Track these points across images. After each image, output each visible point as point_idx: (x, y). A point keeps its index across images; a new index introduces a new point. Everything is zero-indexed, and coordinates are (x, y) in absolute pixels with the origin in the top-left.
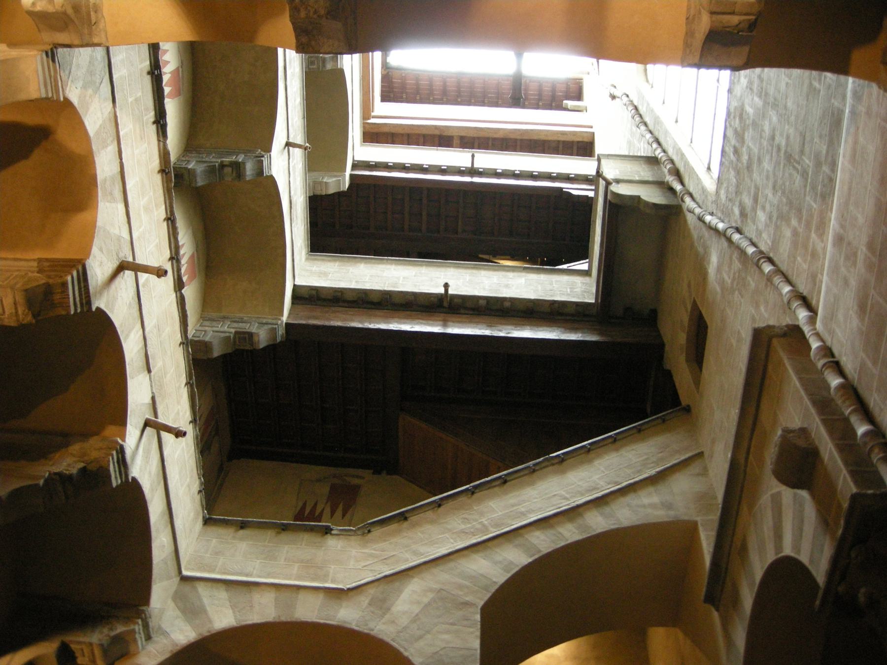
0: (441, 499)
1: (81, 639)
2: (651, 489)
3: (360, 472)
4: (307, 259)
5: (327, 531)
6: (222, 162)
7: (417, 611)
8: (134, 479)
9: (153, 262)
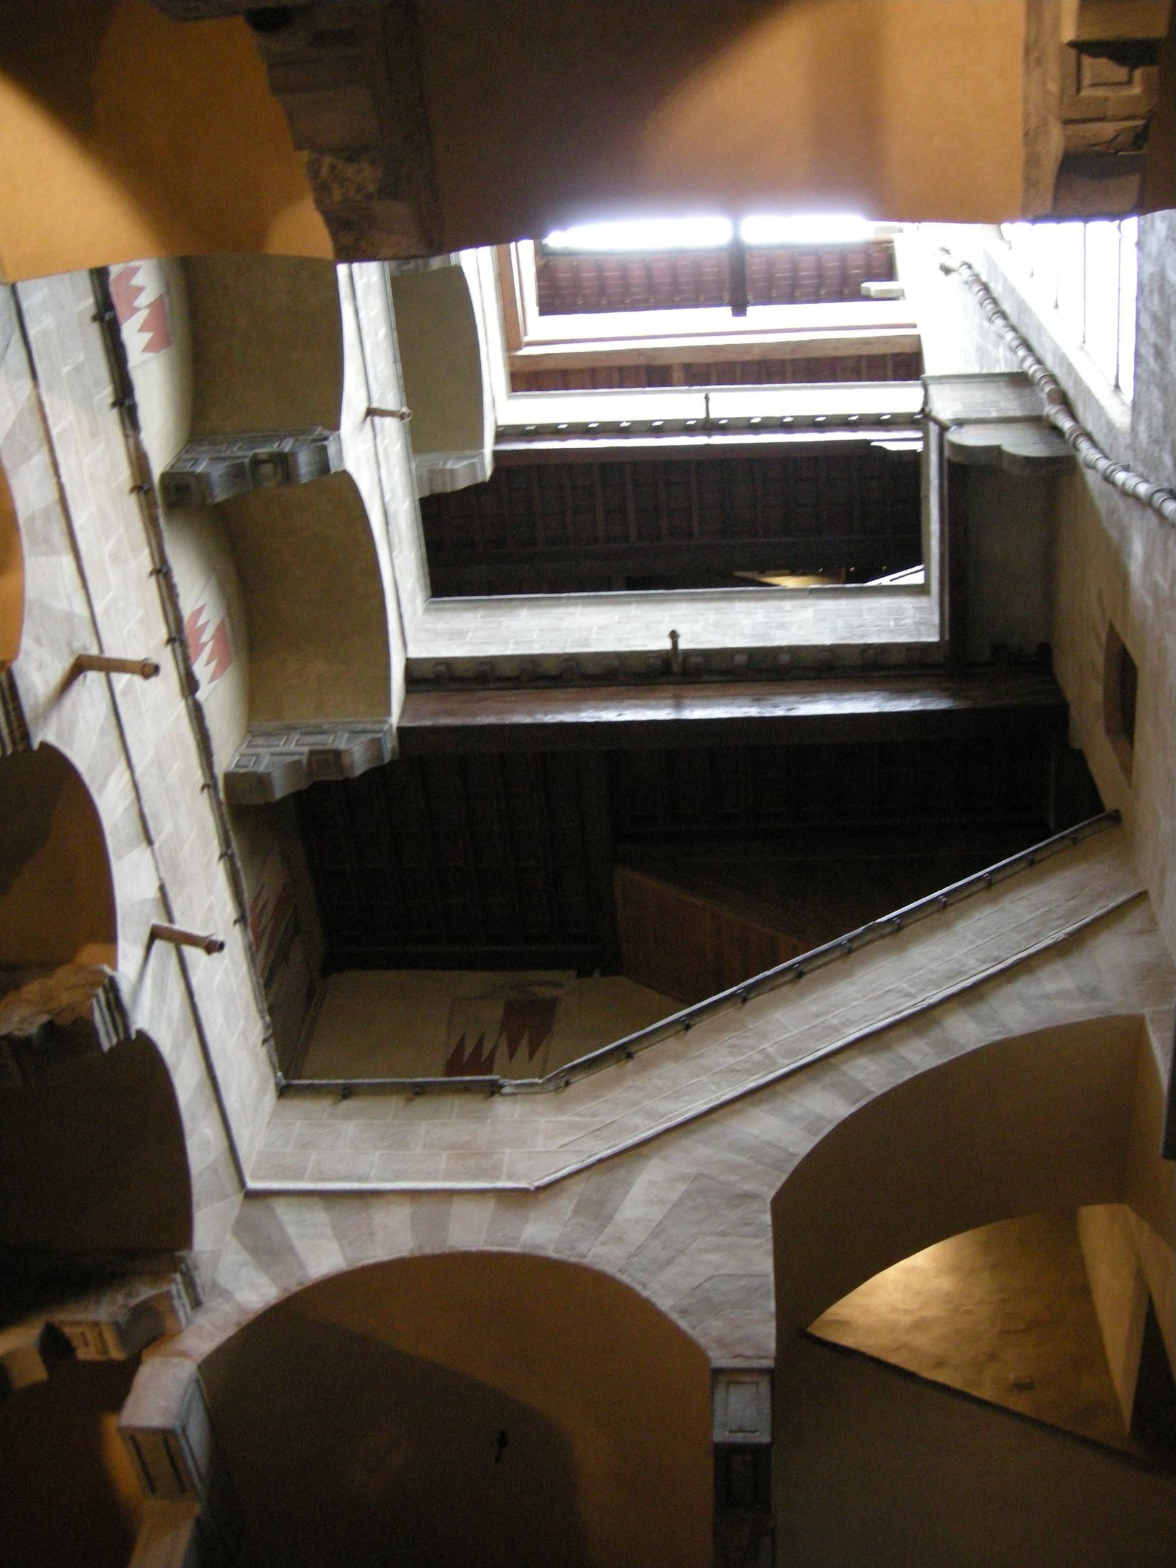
0: (691, 1015)
1: (82, 1316)
2: (1059, 965)
3: (553, 975)
4: (426, 610)
5: (494, 1089)
6: (255, 455)
7: (660, 1217)
8: (141, 1034)
9: (135, 653)
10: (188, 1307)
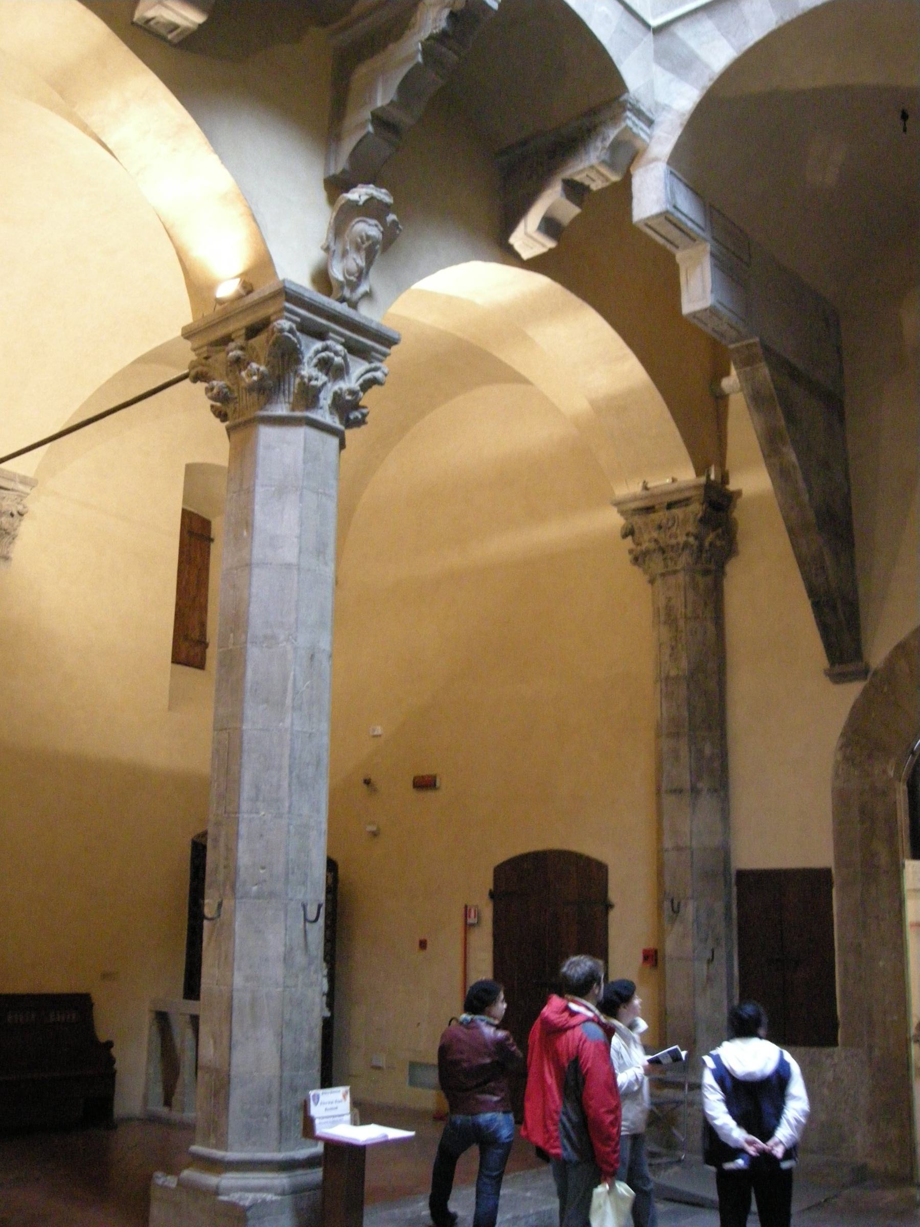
1: (581, 167)
10: (645, 128)
